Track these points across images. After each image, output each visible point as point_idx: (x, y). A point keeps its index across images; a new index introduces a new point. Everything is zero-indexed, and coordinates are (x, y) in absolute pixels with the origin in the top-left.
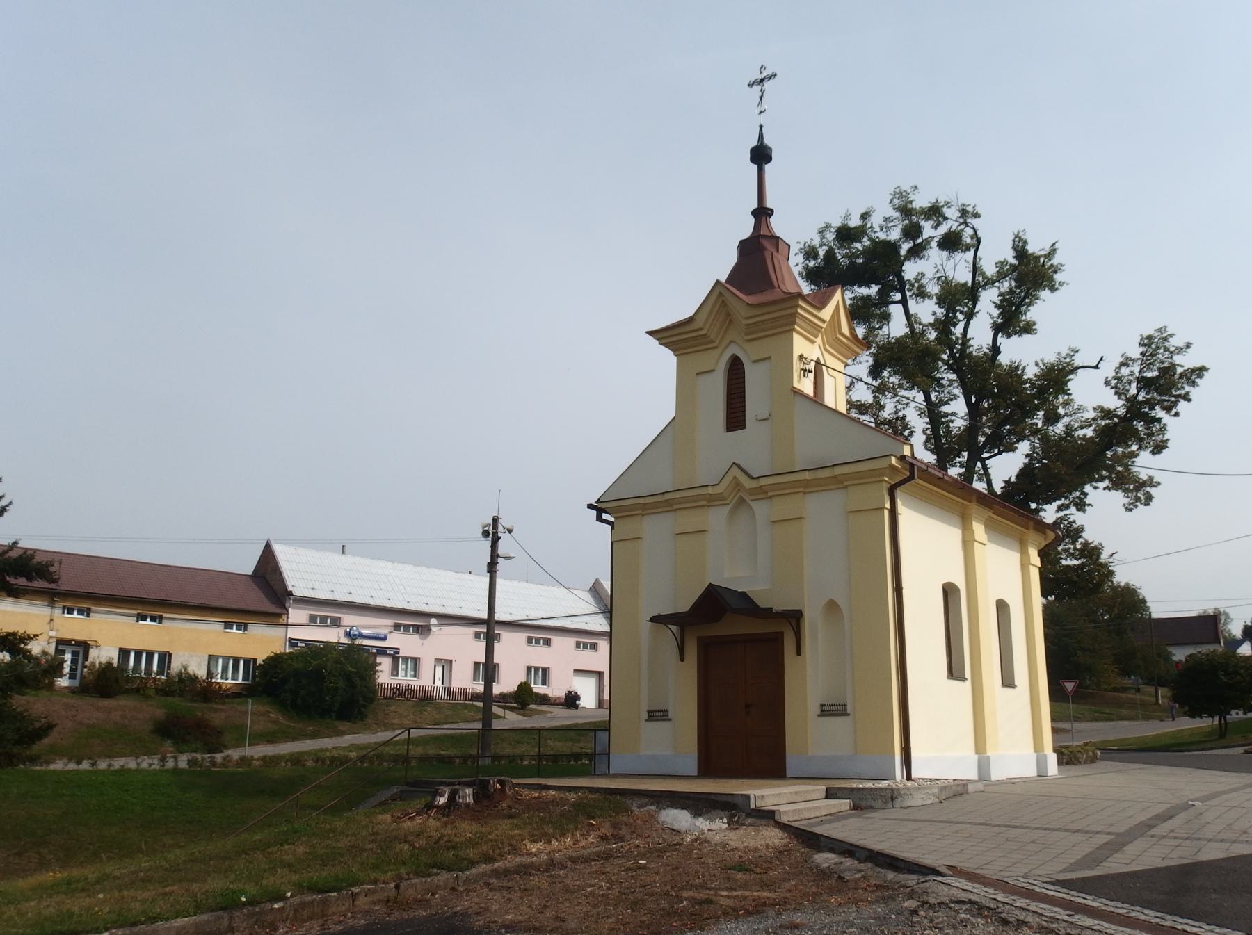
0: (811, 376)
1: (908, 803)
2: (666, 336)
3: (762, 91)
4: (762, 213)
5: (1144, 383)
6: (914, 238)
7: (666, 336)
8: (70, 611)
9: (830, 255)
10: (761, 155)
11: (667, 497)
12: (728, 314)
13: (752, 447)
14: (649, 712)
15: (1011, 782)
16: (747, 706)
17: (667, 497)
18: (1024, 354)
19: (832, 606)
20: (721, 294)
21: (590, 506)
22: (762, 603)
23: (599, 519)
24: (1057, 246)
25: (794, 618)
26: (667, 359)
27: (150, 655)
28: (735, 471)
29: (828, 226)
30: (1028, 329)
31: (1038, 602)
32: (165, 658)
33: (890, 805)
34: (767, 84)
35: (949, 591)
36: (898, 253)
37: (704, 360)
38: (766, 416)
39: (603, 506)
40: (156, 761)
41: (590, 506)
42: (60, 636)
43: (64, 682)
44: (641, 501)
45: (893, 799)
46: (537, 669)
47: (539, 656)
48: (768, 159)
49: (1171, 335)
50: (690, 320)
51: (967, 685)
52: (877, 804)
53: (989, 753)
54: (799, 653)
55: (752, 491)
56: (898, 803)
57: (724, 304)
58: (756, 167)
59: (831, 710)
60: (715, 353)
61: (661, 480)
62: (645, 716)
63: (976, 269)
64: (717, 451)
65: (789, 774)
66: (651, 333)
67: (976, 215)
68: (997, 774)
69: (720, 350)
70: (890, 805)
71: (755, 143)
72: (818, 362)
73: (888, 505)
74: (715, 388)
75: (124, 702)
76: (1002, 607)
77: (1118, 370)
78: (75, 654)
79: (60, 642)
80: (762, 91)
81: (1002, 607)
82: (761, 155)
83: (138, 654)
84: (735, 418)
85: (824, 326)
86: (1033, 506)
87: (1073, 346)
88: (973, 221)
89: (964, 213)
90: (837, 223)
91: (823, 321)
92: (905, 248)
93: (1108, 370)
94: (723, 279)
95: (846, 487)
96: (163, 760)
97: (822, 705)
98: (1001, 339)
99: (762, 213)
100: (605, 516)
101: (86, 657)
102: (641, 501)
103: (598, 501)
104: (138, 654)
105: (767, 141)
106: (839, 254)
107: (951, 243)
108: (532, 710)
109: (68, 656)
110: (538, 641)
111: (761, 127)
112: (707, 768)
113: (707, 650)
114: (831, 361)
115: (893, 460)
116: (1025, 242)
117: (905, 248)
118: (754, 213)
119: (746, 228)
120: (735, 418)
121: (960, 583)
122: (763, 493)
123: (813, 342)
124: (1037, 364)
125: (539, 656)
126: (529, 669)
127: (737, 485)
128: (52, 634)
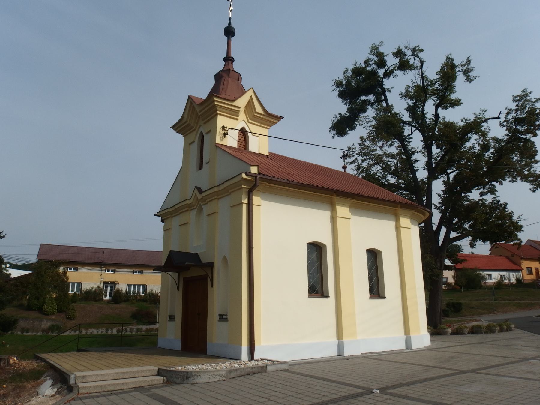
1: (197, 380)
4: (229, 59)
5: (518, 121)
6: (384, 67)
8: (108, 271)
9: (348, 84)
10: (229, 32)
14: (220, 315)
15: (366, 357)
17: (176, 207)
18: (452, 116)
24: (470, 58)
26: (180, 139)
27: (139, 286)
29: (347, 70)
30: (457, 103)
32: (145, 287)
36: (379, 76)
40: (104, 331)
42: (105, 280)
43: (108, 298)
44: (169, 210)
45: (187, 378)
48: (233, 35)
49: (531, 93)
50: (182, 117)
51: (329, 303)
52: (178, 381)
53: (411, 335)
56: (190, 381)
59: (223, 318)
60: (195, 132)
61: (176, 199)
62: (217, 317)
63: (423, 78)
65: (208, 352)
67: (422, 51)
68: (347, 353)
69: (196, 131)
70: (185, 382)
71: (227, 25)
72: (243, 131)
73: (245, 201)
75: (123, 305)
76: (376, 290)
77: (506, 117)
78: (111, 287)
79: (105, 283)
81: (376, 290)
82: (229, 32)
83: (135, 286)
86: (463, 195)
87: (483, 109)
88: (420, 55)
89: (414, 50)
90: (351, 67)
92: (381, 72)
96: (107, 330)
98: (440, 110)
99: (229, 59)
101: (115, 287)
102: (169, 210)
104: (135, 286)
105: (233, 25)
106: (353, 82)
107: (404, 66)
109: (109, 289)
115: (244, 176)
116: (453, 60)
117: (381, 72)
119: (221, 65)
124: (462, 121)
128: (102, 280)
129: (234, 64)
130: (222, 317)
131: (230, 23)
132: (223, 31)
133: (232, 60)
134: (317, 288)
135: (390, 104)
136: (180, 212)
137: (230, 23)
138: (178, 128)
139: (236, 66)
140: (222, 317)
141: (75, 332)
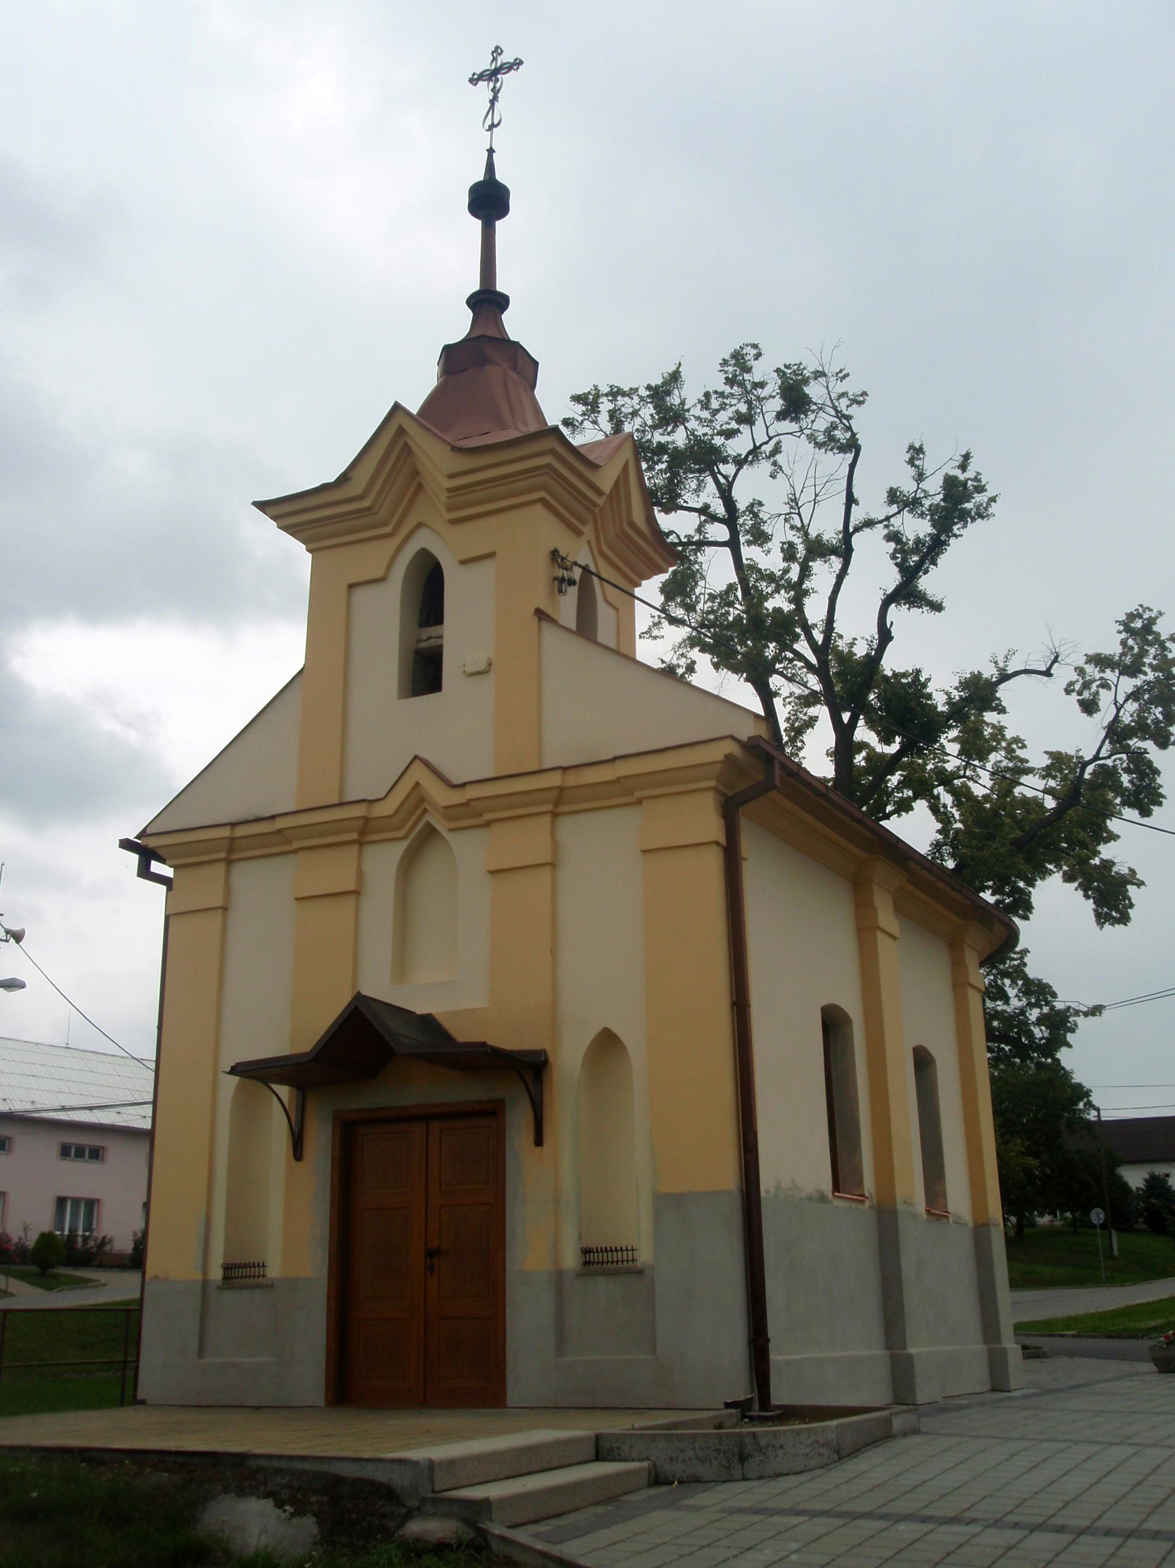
0: (573, 591)
2: (291, 512)
3: (496, 92)
4: (488, 302)
7: (291, 512)
10: (489, 201)
11: (280, 824)
12: (416, 473)
13: (460, 733)
16: (431, 1254)
17: (280, 824)
18: (931, 654)
19: (607, 1044)
20: (401, 431)
21: (126, 844)
22: (463, 1033)
23: (144, 872)
25: (531, 1069)
28: (419, 774)
31: (982, 1056)
33: (737, 1472)
34: (506, 79)
35: (833, 1023)
37: (368, 559)
38: (482, 666)
39: (152, 843)
41: (126, 844)
45: (742, 1458)
46: (76, 1201)
47: (80, 1179)
54: (539, 1142)
55: (451, 812)
57: (407, 450)
58: (478, 223)
60: (392, 544)
61: (276, 792)
64: (390, 737)
66: (262, 506)
71: (480, 176)
74: (384, 614)
76: (923, 1061)
80: (496, 92)
81: (923, 1061)
82: (489, 201)
84: (425, 672)
85: (600, 501)
91: (599, 493)
93: (1064, 674)
94: (414, 406)
95: (639, 802)
97: (586, 1251)
99: (488, 302)
100: (156, 867)
103: (141, 835)
108: (56, 1276)
110: (80, 1153)
111: (491, 151)
112: (346, 1388)
113: (349, 1136)
114: (606, 571)
118: (474, 302)
119: (459, 324)
120: (425, 672)
121: (852, 1006)
122: (472, 814)
123: (578, 533)
125: (80, 1179)
126: (61, 1201)
127: (417, 801)
129: (506, 317)
130: (593, 1257)
131: (490, 168)
132: (465, 200)
133: (502, 302)
134: (96, 1154)
135: (990, 510)
136: (297, 844)
137: (490, 168)
138: (288, 515)
139: (514, 324)
140: (593, 1257)
141: (887, 740)
